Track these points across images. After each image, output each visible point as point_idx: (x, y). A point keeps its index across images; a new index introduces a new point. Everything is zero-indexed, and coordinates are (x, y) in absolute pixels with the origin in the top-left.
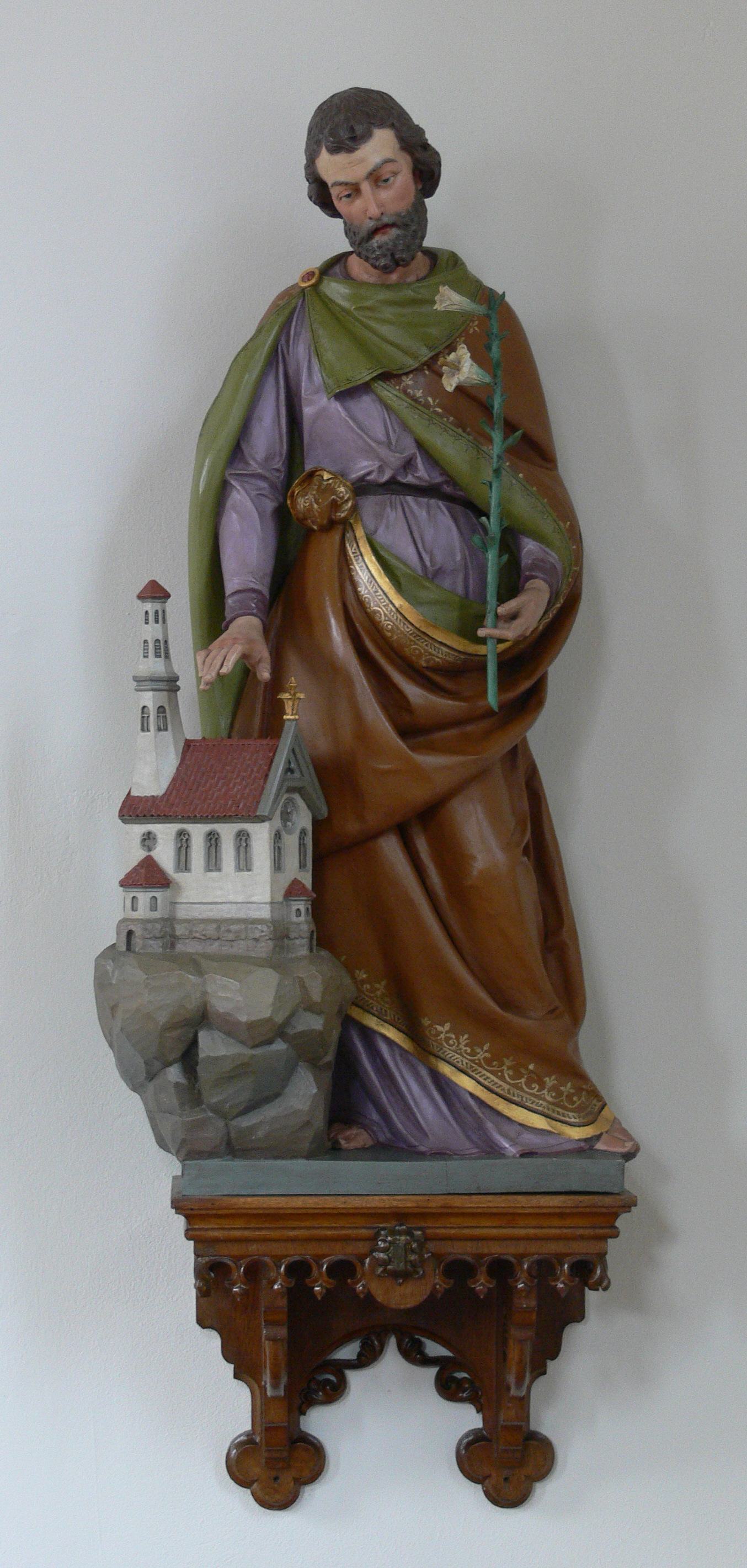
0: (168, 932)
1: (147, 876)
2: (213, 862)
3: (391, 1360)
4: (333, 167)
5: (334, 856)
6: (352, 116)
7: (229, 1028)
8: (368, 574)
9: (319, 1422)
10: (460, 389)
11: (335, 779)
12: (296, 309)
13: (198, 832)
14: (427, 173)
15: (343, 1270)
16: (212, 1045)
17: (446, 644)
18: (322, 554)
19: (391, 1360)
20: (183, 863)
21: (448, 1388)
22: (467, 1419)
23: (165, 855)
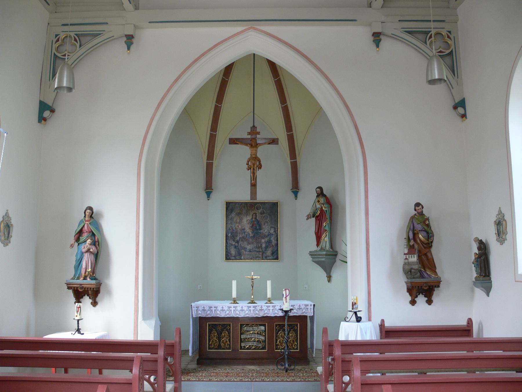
0: (408, 263)
1: (406, 259)
3: (421, 294)
4: (417, 208)
5: (419, 257)
6: (418, 205)
7: (414, 269)
8: (420, 236)
9: (416, 299)
11: (419, 251)
12: (412, 218)
14: (423, 207)
16: (413, 271)
17: (426, 242)
18: (416, 235)
19: (421, 294)
21: (425, 297)
22: (426, 299)
23: (408, 257)
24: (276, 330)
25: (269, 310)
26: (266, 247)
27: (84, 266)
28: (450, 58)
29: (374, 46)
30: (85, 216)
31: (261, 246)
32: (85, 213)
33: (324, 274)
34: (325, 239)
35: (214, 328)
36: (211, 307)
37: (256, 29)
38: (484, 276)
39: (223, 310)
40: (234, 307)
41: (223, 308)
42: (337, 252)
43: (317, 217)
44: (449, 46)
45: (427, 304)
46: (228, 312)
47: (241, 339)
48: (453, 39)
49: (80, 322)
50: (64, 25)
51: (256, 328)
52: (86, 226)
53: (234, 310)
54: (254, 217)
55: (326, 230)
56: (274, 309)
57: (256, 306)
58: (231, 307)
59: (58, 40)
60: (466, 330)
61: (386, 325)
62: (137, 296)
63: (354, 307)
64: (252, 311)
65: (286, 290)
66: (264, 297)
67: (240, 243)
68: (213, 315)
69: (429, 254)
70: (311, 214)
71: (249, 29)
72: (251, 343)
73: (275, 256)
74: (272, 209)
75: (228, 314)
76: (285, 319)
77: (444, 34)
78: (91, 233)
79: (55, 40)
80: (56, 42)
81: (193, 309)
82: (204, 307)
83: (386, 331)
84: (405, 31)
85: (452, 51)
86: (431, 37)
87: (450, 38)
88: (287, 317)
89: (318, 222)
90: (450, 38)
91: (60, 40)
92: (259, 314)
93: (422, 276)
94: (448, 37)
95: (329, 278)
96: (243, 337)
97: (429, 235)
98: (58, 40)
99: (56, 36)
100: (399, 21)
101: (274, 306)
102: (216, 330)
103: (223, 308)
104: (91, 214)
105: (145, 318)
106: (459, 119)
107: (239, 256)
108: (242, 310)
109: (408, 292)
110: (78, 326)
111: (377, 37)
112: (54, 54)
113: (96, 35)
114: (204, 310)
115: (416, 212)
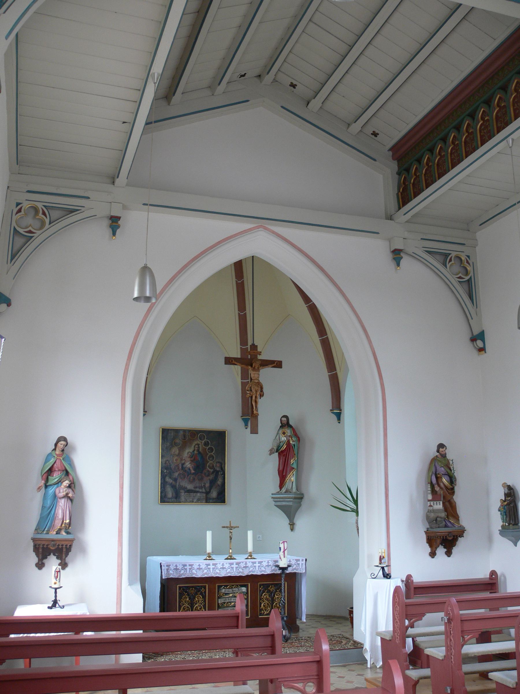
1: (431, 506)
2: (437, 504)
3: (440, 546)
7: (441, 518)
8: (444, 480)
9: (45, 561)
10: (195, 470)
12: (434, 460)
13: (435, 502)
15: (446, 537)
16: (438, 519)
18: (439, 479)
20: (434, 504)
21: (445, 548)
22: (446, 550)
23: (432, 504)
24: (260, 591)
25: (255, 567)
26: (211, 488)
27: (60, 516)
28: (468, 287)
29: (393, 264)
30: (55, 449)
31: (205, 486)
32: (56, 445)
33: (286, 521)
34: (292, 478)
35: (186, 592)
36: (186, 565)
37: (266, 229)
38: (514, 525)
39: (199, 569)
40: (213, 564)
41: (199, 565)
42: (303, 494)
43: (282, 452)
44: (467, 273)
45: (446, 556)
46: (205, 571)
47: (218, 604)
48: (471, 264)
49: (58, 590)
50: (29, 192)
51: (236, 589)
52: (58, 462)
53: (213, 568)
54: (196, 449)
55: (294, 468)
56: (262, 565)
57: (217, 564)
58: (209, 565)
59: (20, 211)
60: (491, 583)
61: (414, 581)
62: (120, 555)
63: (383, 561)
64: (235, 569)
65: (284, 542)
66: (243, 550)
67: (179, 480)
68: (188, 575)
69: (452, 500)
70: (275, 448)
71: (258, 227)
72: (230, 608)
73: (221, 499)
74: (217, 440)
75: (206, 573)
76: (281, 577)
77: (463, 259)
78: (65, 472)
79: (15, 212)
80: (17, 213)
81: (163, 568)
82: (176, 566)
83: (415, 588)
84: (426, 251)
85: (471, 277)
86: (450, 260)
87: (469, 264)
88: (283, 575)
89: (283, 458)
90: (469, 264)
91: (22, 210)
92: (242, 573)
93: (446, 526)
94: (468, 262)
95: (292, 526)
96: (220, 601)
97: (452, 480)
98: (20, 211)
99: (18, 204)
100: (422, 239)
101: (238, 564)
102: (188, 595)
103: (199, 566)
104: (63, 446)
105: (131, 583)
106: (475, 352)
107: (176, 499)
108: (223, 568)
109: (427, 543)
110: (56, 596)
111: (397, 255)
112: (15, 228)
113: (72, 211)
114: (176, 569)
115: (438, 454)
